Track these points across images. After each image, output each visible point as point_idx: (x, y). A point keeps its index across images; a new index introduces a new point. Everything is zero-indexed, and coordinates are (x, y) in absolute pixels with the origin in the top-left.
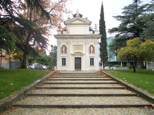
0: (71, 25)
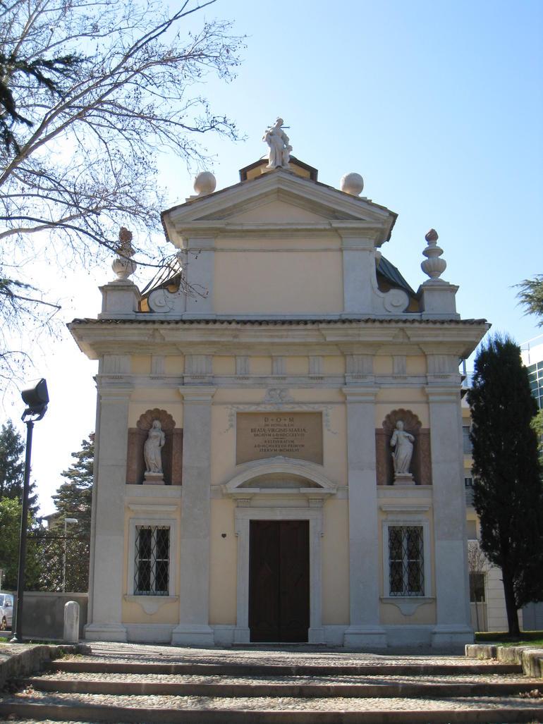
0: (220, 243)
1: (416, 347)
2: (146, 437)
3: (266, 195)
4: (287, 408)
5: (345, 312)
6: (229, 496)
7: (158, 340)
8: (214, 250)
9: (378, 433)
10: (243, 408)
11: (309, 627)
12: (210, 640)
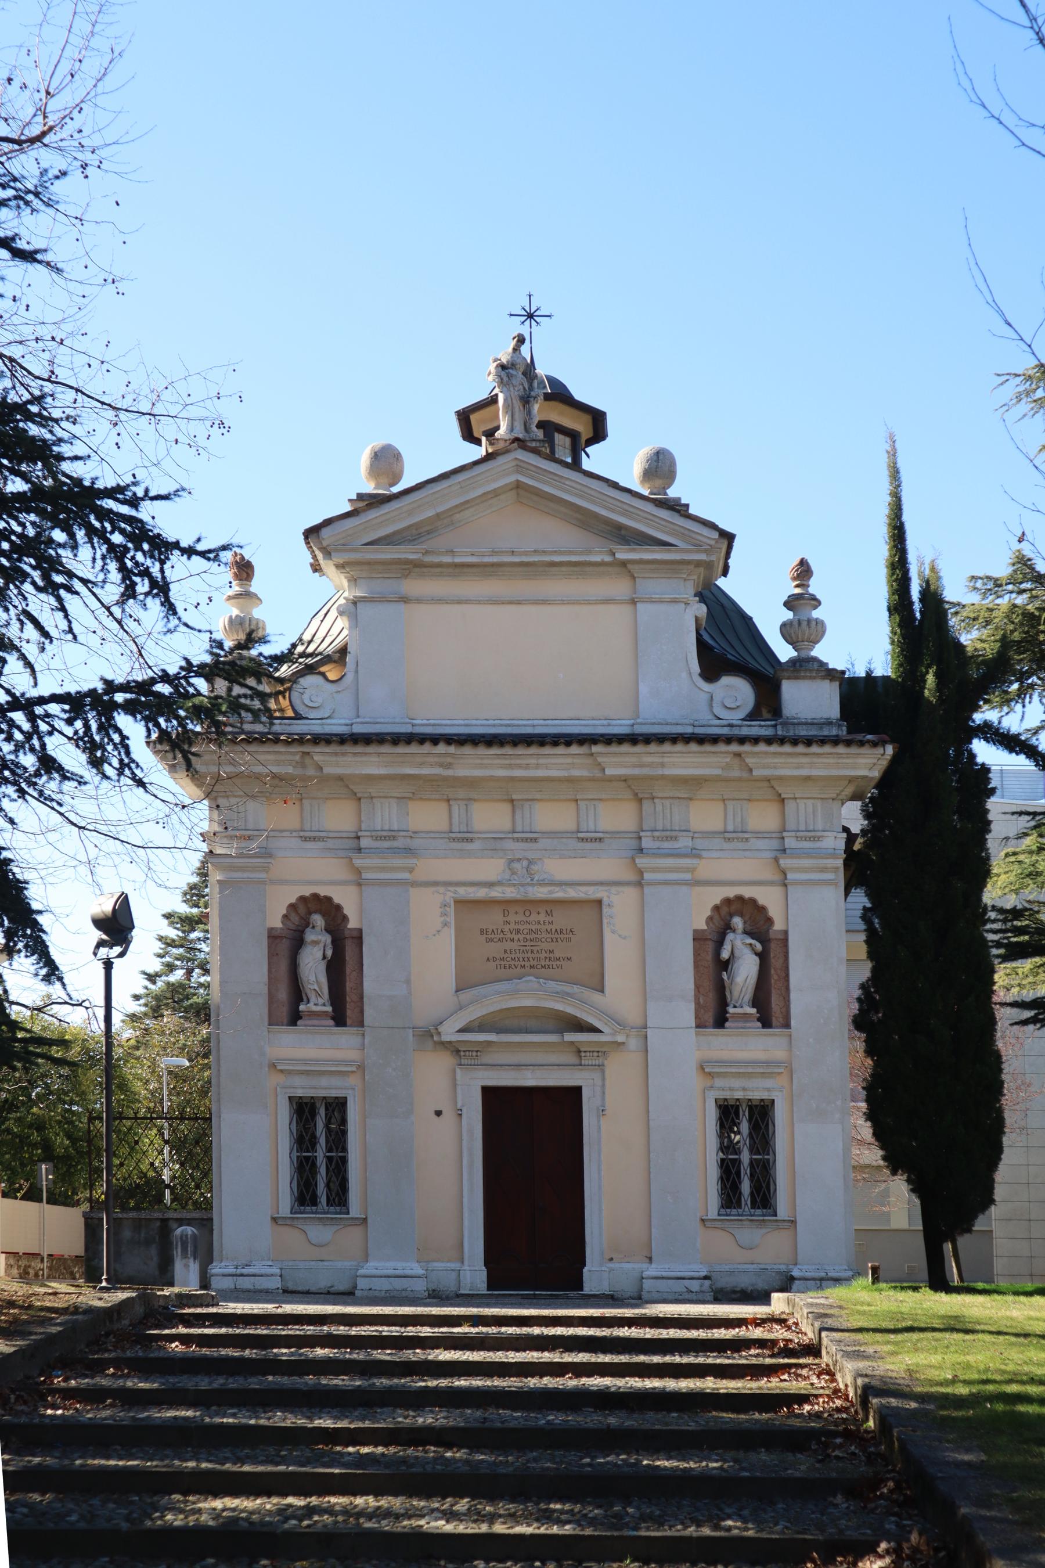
0: (413, 586)
1: (766, 784)
2: (298, 942)
3: (495, 493)
4: (541, 893)
5: (639, 721)
6: (445, 1045)
7: (311, 772)
8: (404, 600)
9: (698, 938)
10: (463, 892)
11: (584, 1264)
12: (420, 1287)
